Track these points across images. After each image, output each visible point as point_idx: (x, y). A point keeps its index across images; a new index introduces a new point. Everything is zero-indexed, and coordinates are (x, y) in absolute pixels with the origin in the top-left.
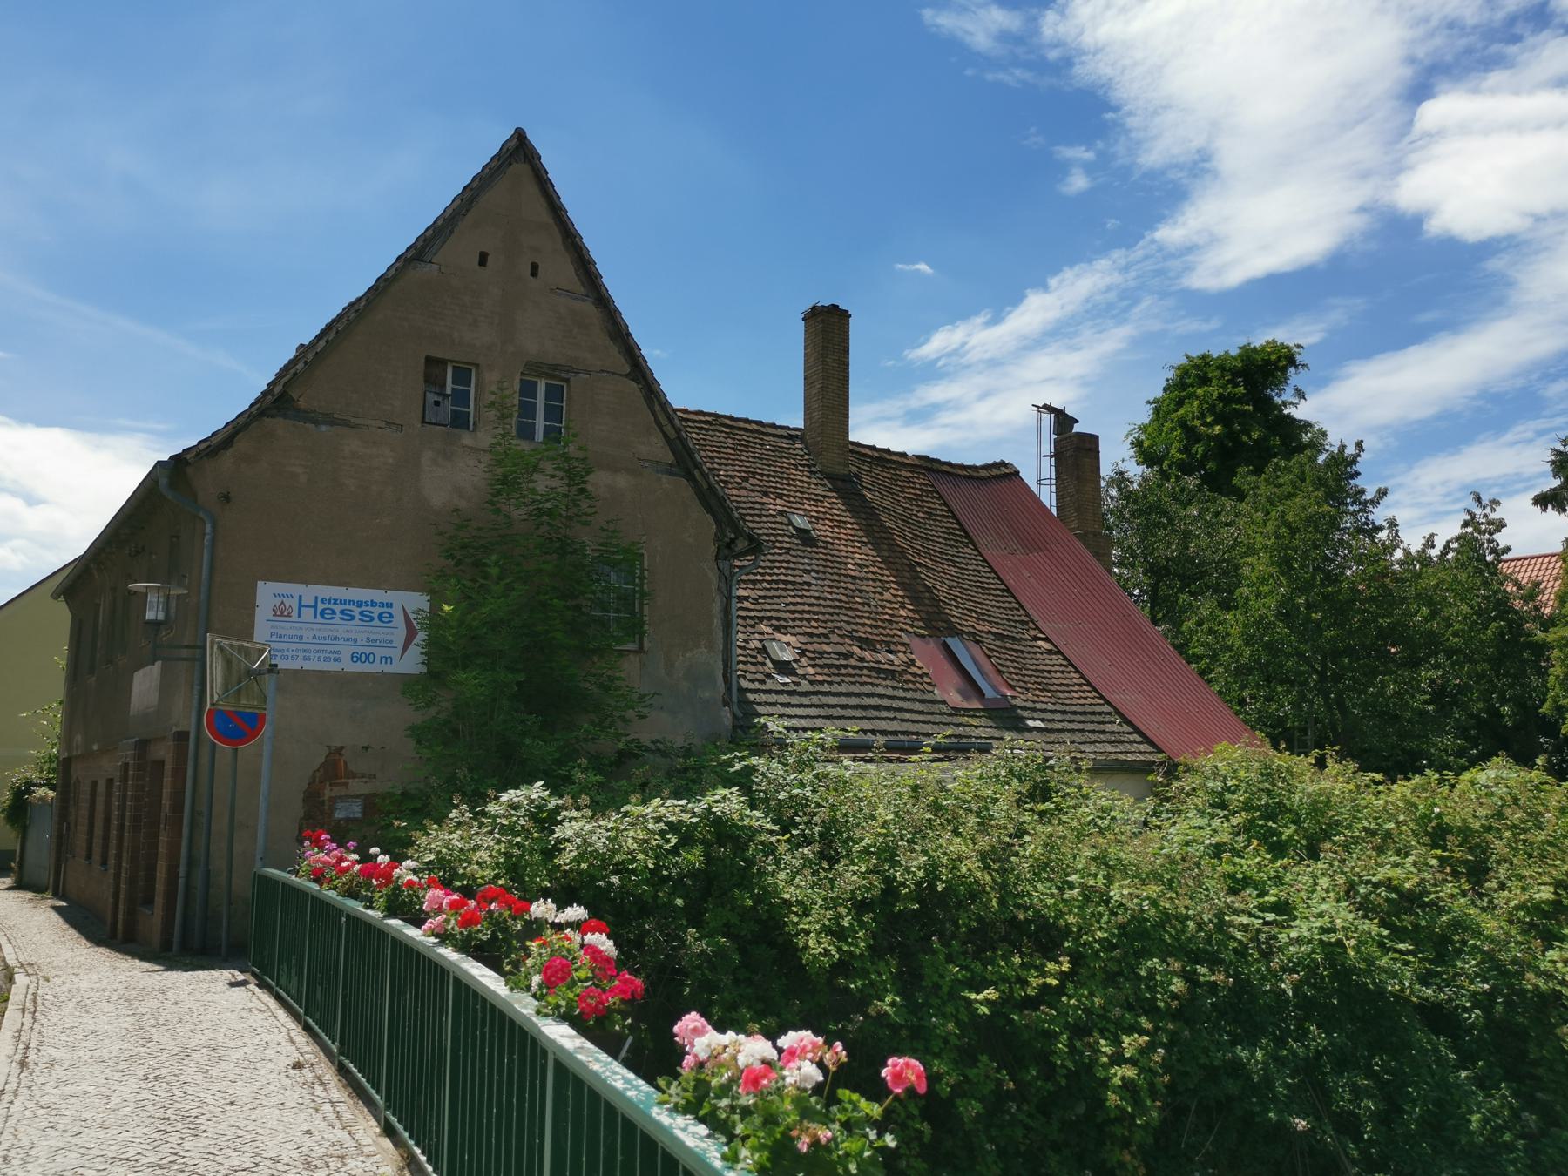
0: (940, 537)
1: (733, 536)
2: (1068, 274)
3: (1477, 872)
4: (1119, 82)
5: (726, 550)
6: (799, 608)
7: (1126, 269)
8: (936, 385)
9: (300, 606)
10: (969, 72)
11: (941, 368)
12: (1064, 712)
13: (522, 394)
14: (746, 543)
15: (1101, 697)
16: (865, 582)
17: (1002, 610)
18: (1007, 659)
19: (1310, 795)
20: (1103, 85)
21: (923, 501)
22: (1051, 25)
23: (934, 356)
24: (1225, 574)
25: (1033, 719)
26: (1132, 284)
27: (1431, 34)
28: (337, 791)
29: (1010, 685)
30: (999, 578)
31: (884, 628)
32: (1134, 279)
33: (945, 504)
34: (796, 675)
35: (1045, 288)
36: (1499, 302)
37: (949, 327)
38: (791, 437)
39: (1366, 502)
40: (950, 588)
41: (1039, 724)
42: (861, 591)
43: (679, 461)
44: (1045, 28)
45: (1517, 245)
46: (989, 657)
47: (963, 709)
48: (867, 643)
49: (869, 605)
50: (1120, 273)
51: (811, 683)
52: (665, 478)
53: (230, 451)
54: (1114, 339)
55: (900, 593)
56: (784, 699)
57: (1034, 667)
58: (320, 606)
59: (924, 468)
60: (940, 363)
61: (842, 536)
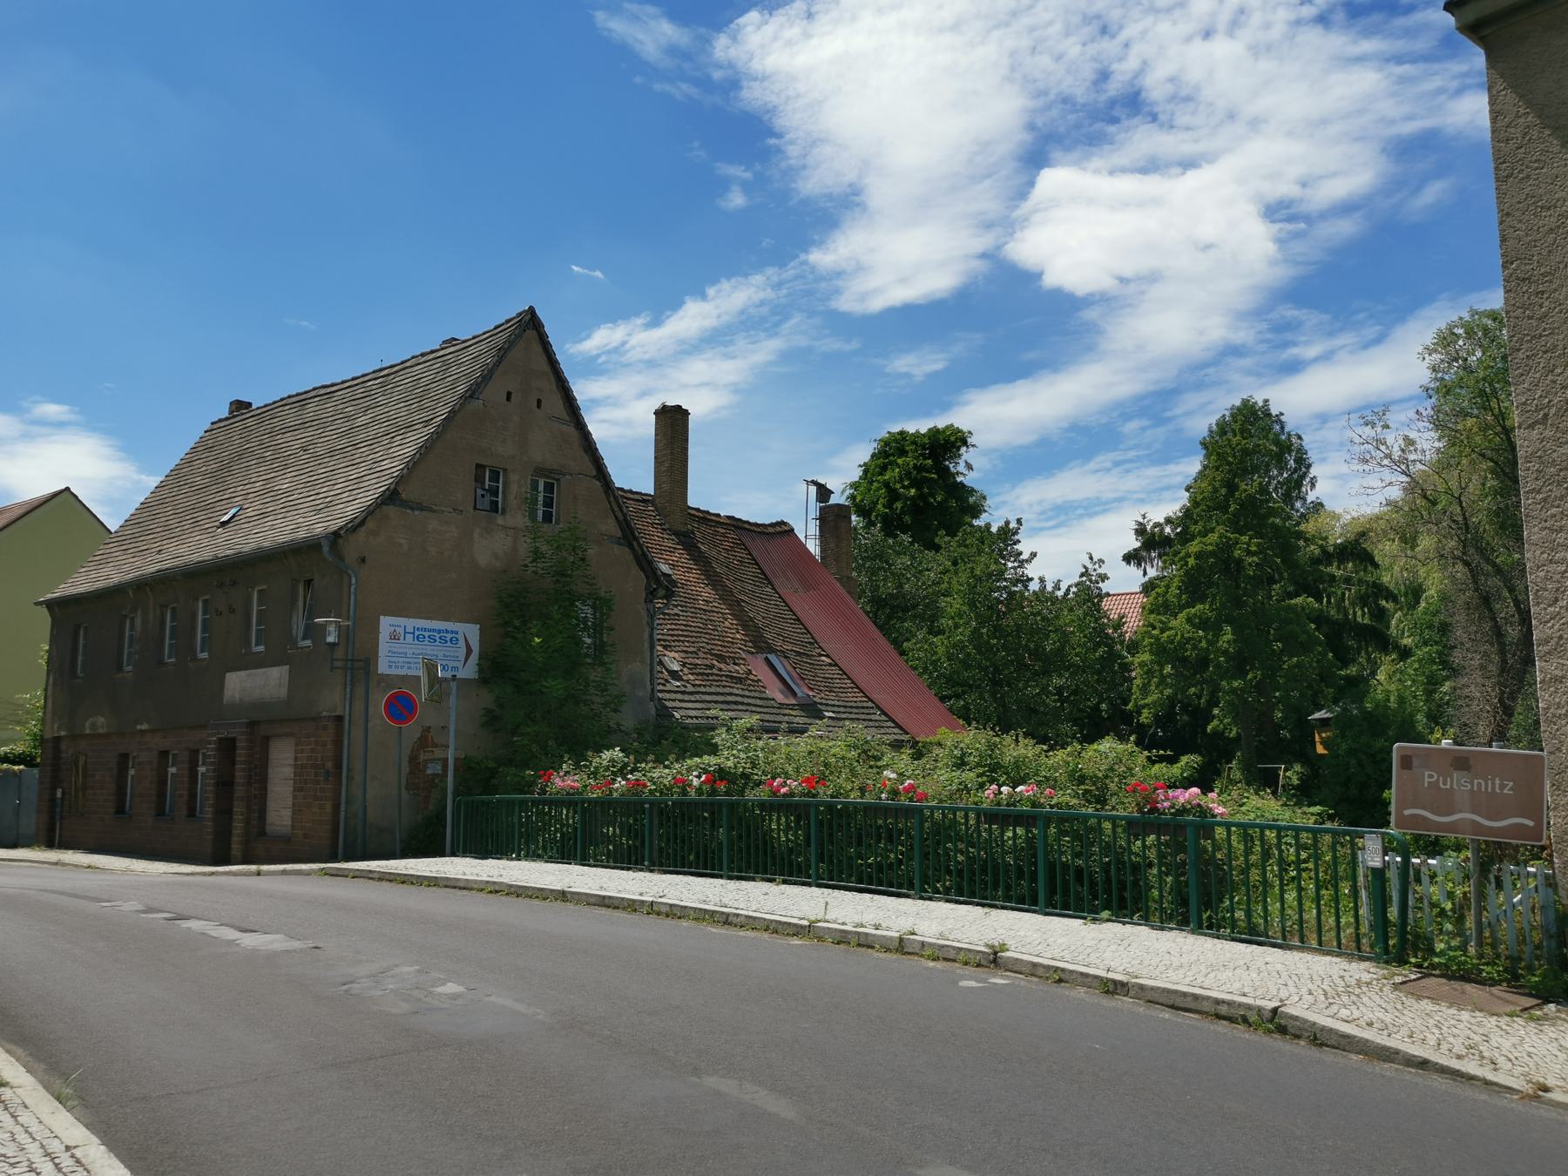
0: (750, 579)
1: (655, 587)
2: (725, 285)
3: (1101, 801)
4: (782, 111)
5: (651, 594)
6: (676, 632)
7: (778, 286)
8: (596, 381)
9: (405, 633)
10: (638, 80)
11: (600, 364)
12: (845, 707)
13: (552, 499)
14: (664, 592)
15: (866, 696)
16: (712, 614)
17: (796, 635)
18: (806, 670)
19: (1015, 757)
20: (768, 111)
21: (735, 552)
22: (722, 47)
23: (595, 352)
24: (926, 606)
25: (827, 711)
26: (783, 301)
27: (1049, 107)
28: (428, 756)
29: (810, 688)
30: (792, 611)
31: (729, 647)
32: (785, 297)
33: (750, 554)
34: (683, 680)
35: (704, 296)
36: (1090, 348)
37: (610, 325)
38: (644, 501)
39: (1023, 560)
40: (763, 618)
41: (831, 714)
42: (711, 621)
43: (625, 537)
44: (717, 50)
45: (1107, 300)
46: (795, 668)
47: (791, 705)
48: (721, 658)
49: (717, 631)
50: (772, 289)
51: (694, 685)
52: (616, 547)
53: (362, 529)
54: (766, 350)
55: (735, 622)
56: (679, 696)
57: (822, 675)
58: (417, 633)
59: (733, 526)
60: (601, 360)
61: (691, 579)
